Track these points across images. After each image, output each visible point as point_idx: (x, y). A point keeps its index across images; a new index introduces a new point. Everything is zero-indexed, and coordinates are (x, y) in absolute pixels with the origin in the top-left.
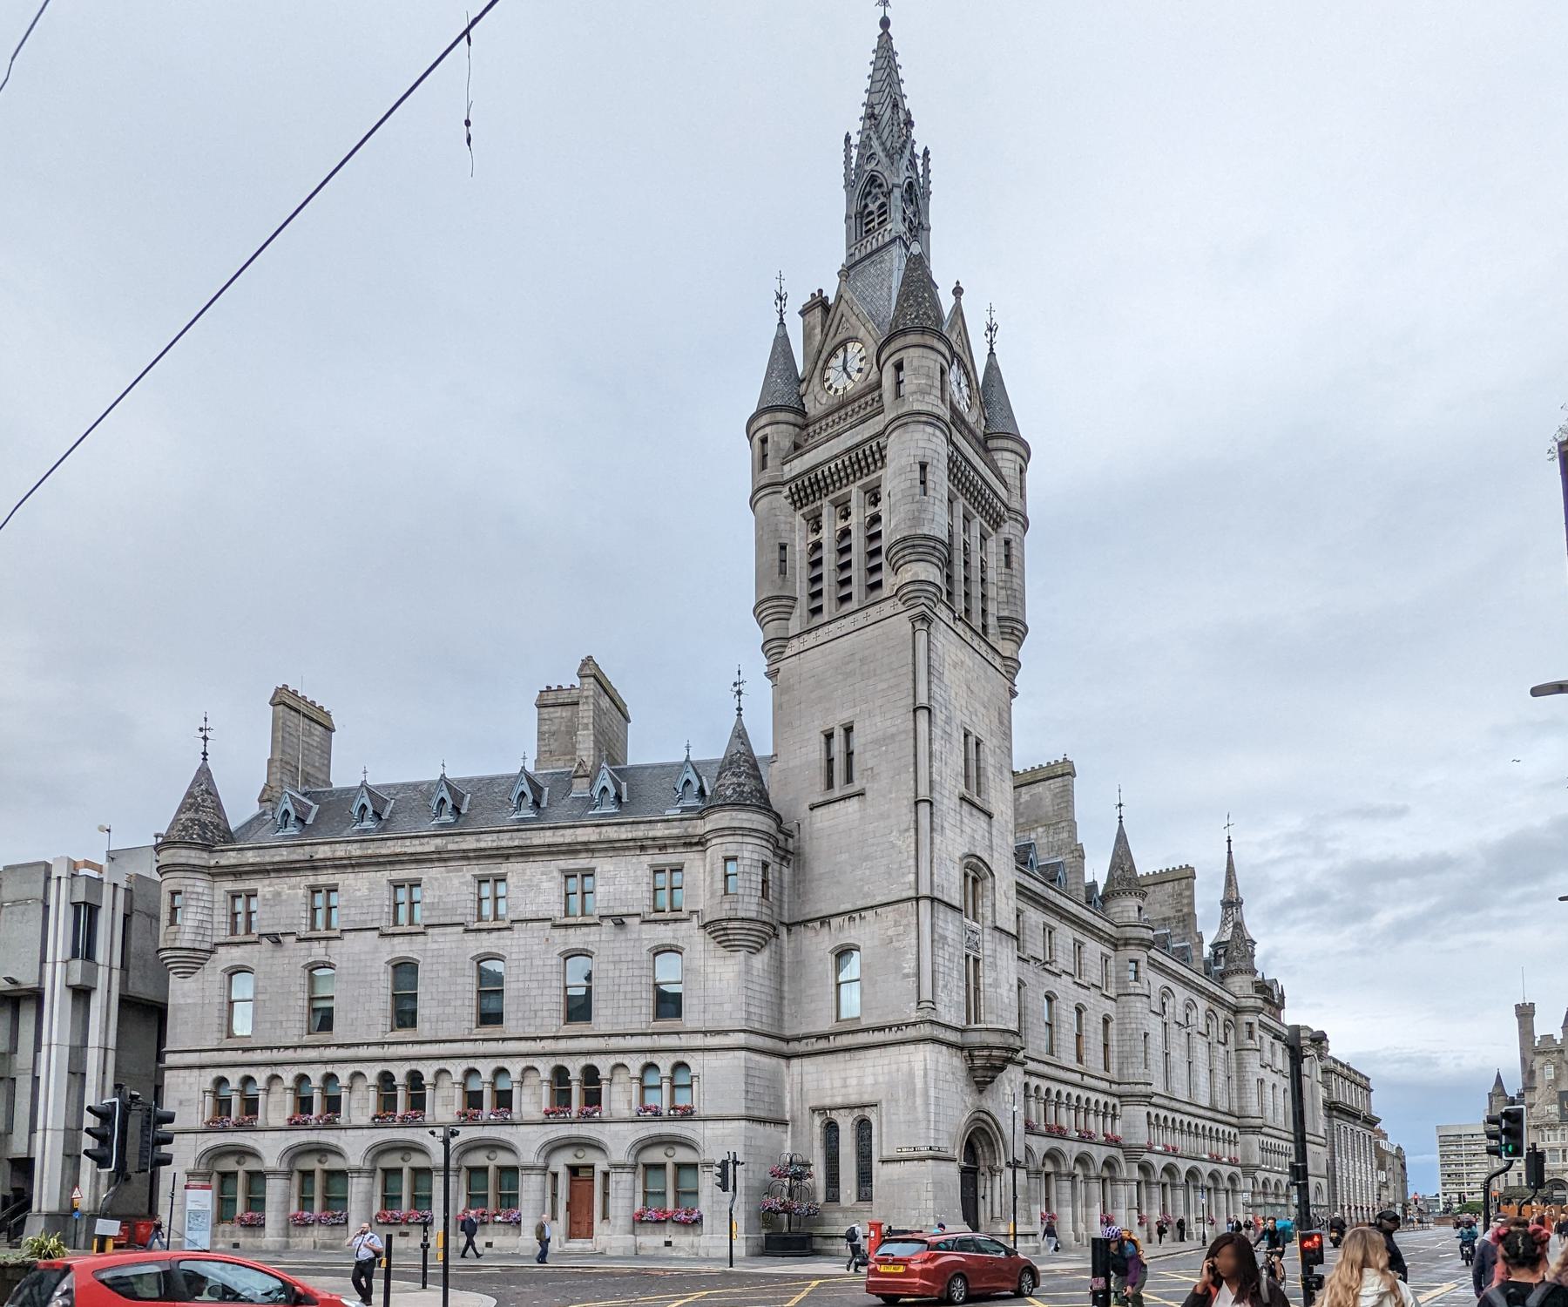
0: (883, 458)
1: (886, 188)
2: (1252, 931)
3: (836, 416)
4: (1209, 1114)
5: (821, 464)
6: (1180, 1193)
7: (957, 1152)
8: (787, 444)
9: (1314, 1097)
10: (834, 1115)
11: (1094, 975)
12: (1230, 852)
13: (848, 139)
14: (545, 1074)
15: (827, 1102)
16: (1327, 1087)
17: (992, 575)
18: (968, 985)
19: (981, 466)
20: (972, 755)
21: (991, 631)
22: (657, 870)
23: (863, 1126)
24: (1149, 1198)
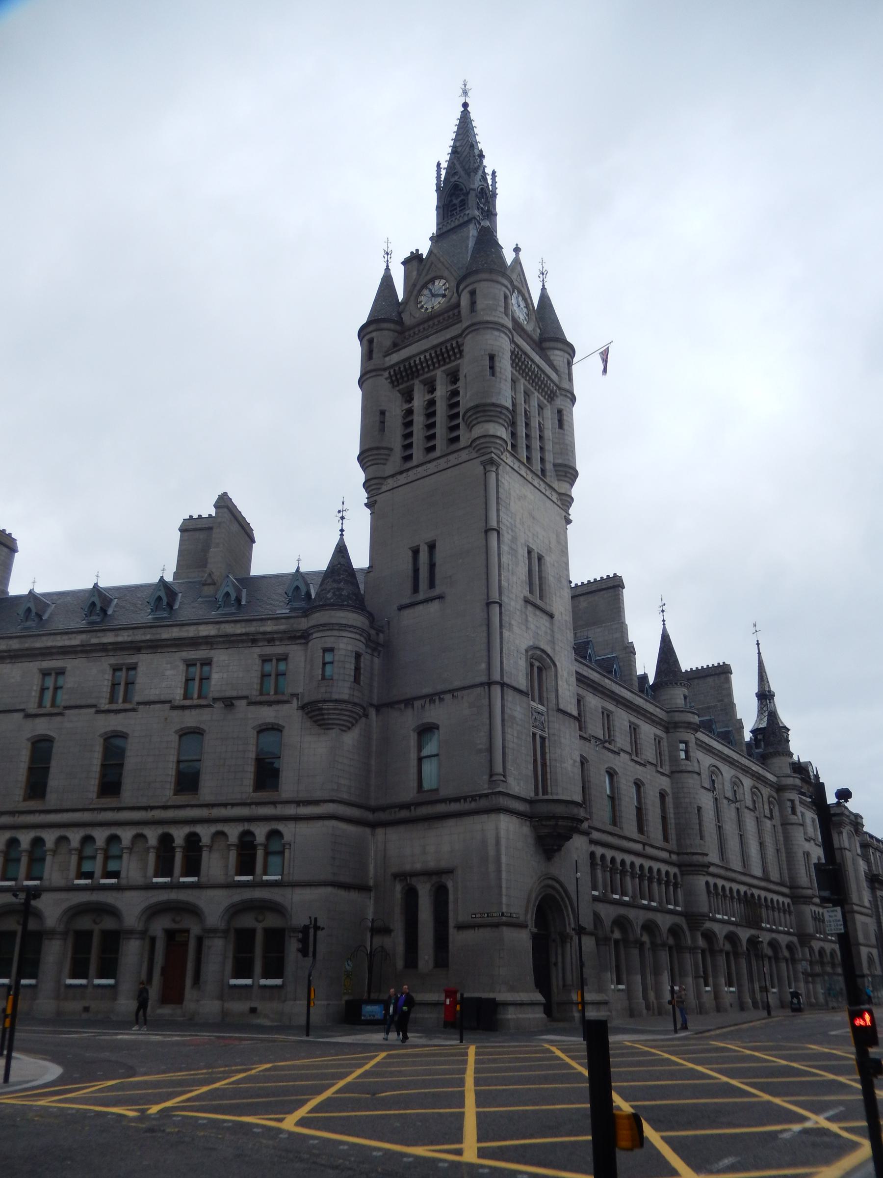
0: (461, 352)
1: (464, 192)
2: (785, 717)
3: (426, 325)
4: (763, 884)
5: (414, 356)
6: (743, 962)
7: (530, 919)
8: (388, 343)
9: (856, 870)
10: (414, 881)
11: (649, 753)
12: (759, 653)
13: (439, 164)
14: (153, 841)
15: (408, 867)
16: (866, 858)
17: (548, 434)
18: (535, 761)
19: (537, 359)
20: (536, 568)
21: (548, 474)
22: (265, 660)
23: (441, 895)
24: (714, 966)
